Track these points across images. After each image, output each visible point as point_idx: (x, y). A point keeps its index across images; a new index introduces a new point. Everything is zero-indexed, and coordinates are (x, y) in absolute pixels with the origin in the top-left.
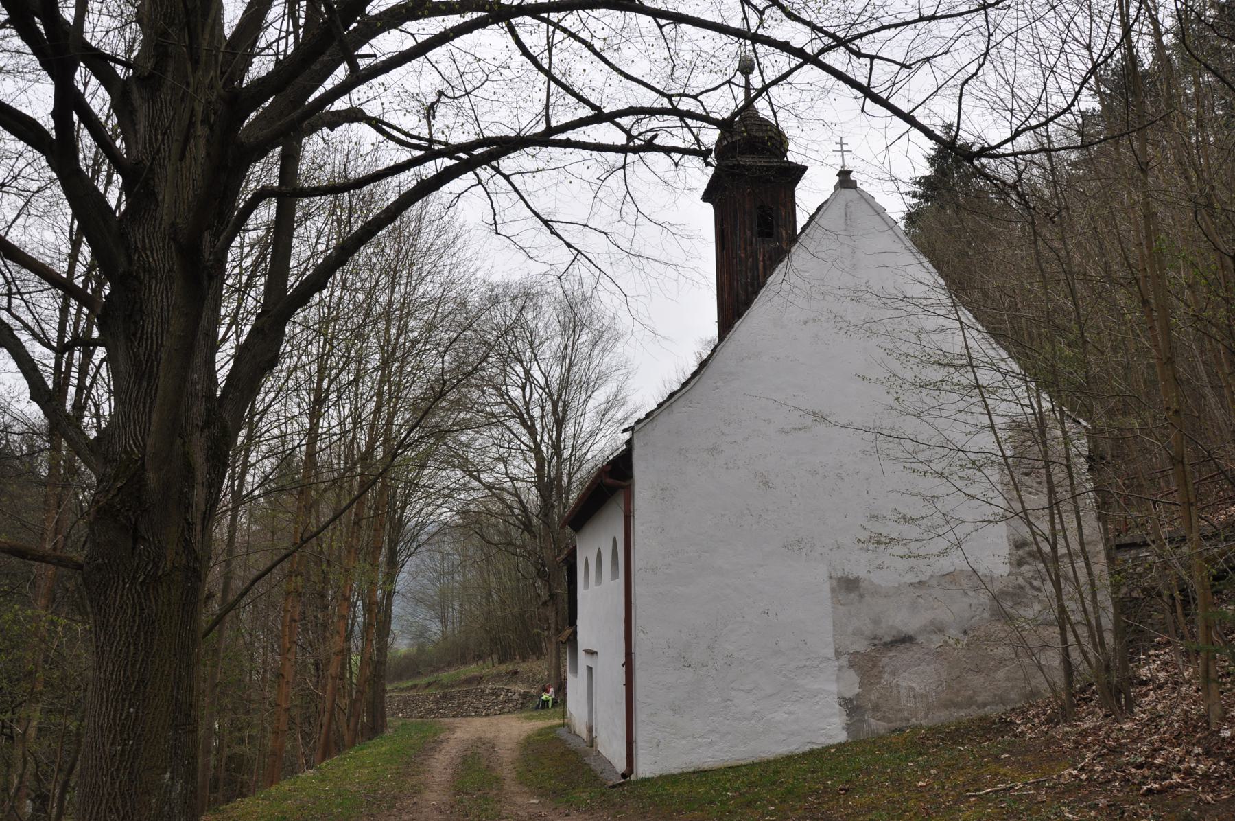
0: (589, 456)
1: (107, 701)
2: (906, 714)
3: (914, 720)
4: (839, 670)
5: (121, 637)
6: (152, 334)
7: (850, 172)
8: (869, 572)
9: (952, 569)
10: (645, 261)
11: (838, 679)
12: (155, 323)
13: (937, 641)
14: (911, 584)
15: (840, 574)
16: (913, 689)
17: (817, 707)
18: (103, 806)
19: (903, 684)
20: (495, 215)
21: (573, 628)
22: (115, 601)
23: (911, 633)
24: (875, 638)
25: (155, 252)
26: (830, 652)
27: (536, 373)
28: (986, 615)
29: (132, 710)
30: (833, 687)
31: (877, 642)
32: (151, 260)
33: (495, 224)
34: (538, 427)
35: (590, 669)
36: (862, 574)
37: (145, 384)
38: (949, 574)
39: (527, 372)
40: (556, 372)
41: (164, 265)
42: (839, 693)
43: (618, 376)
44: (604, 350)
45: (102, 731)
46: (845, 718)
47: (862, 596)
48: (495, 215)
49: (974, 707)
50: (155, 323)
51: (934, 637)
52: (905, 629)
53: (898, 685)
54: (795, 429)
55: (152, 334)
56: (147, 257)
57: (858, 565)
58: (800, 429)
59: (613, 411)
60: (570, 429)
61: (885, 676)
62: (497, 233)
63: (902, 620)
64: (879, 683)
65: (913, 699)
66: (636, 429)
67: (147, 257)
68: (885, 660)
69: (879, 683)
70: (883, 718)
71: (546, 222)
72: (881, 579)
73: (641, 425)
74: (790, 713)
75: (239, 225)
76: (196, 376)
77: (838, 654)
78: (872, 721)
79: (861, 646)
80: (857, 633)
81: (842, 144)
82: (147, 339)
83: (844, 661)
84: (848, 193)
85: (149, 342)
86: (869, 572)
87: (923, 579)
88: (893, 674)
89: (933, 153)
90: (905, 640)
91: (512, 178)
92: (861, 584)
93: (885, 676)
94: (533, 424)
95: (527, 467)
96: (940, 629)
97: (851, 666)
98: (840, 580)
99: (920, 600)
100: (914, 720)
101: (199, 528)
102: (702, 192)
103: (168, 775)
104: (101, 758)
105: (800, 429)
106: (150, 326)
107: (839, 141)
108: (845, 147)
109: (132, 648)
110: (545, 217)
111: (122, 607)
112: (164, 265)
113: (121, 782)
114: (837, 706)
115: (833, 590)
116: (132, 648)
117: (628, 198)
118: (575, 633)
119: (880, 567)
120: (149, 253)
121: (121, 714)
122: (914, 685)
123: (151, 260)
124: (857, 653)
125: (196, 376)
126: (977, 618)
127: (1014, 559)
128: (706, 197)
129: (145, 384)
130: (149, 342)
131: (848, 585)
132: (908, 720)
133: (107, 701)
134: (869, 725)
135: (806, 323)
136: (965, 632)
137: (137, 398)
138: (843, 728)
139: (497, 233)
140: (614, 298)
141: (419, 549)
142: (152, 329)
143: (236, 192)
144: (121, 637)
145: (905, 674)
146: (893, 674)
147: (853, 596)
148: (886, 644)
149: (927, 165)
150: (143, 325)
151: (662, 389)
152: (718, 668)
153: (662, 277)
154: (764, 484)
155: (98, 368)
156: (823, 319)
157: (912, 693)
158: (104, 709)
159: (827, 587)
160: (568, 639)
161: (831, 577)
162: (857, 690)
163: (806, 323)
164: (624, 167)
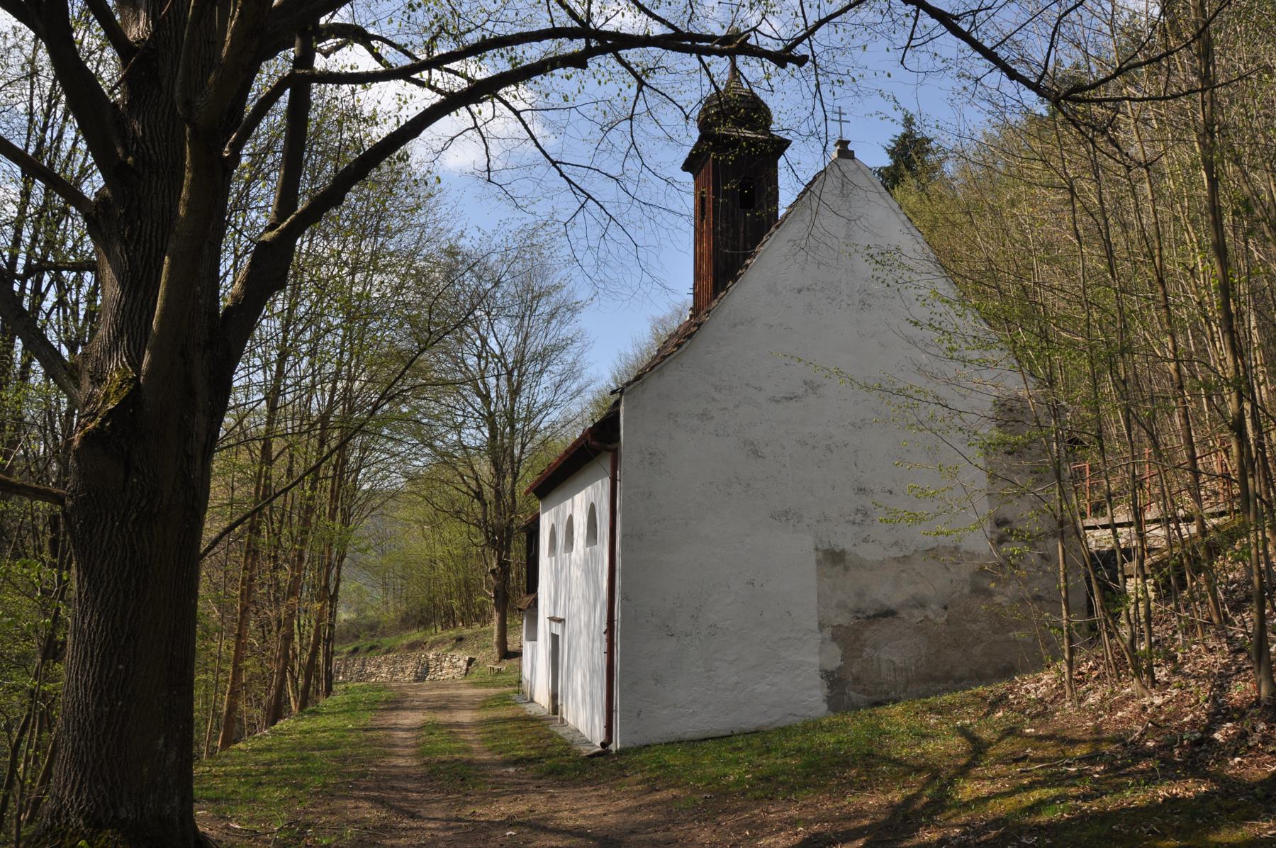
0: (542, 426)
1: (92, 656)
2: (885, 687)
3: (893, 693)
4: (822, 643)
5: (109, 583)
6: (151, 236)
7: (848, 142)
8: (855, 545)
9: (935, 545)
10: (655, 210)
11: (820, 653)
12: (155, 225)
13: (918, 615)
14: (895, 558)
15: (826, 546)
16: (893, 662)
17: (800, 679)
18: (88, 774)
19: (884, 656)
20: (489, 161)
21: (531, 597)
22: (102, 542)
23: (893, 607)
24: (858, 612)
25: (156, 143)
26: (814, 625)
27: (492, 343)
28: (966, 591)
29: (121, 667)
30: (816, 660)
31: (860, 615)
32: (152, 152)
33: (489, 170)
34: (493, 395)
35: (555, 638)
36: (848, 546)
37: (141, 294)
38: (933, 549)
39: (484, 341)
40: (513, 341)
41: (167, 159)
42: (821, 665)
43: (573, 349)
44: (562, 322)
45: (86, 691)
46: (826, 690)
47: (847, 569)
48: (489, 161)
49: (951, 682)
50: (155, 225)
51: (916, 612)
52: (887, 603)
53: (879, 659)
54: (786, 398)
55: (151, 236)
56: (148, 149)
57: (844, 539)
58: (791, 399)
59: (568, 383)
60: (523, 400)
61: (867, 649)
62: (489, 180)
63: (885, 593)
64: (861, 656)
65: (892, 673)
66: (626, 390)
67: (148, 149)
68: (867, 634)
69: (861, 656)
70: (864, 691)
71: (554, 163)
72: (869, 553)
73: (631, 386)
74: (773, 685)
75: (247, 132)
76: (199, 288)
77: (821, 626)
78: (852, 693)
79: (844, 619)
80: (841, 605)
81: (840, 114)
82: (145, 242)
83: (827, 633)
84: (846, 164)
85: (148, 245)
86: (855, 545)
87: (908, 554)
88: (875, 647)
89: (893, 145)
90: (889, 613)
91: (522, 115)
92: (847, 557)
93: (867, 649)
94: (488, 392)
95: (479, 436)
96: (922, 604)
97: (834, 638)
98: (826, 552)
99: (904, 575)
100: (893, 693)
101: (199, 462)
102: (682, 161)
103: (161, 741)
104: (85, 721)
105: (791, 399)
106: (149, 228)
107: (837, 110)
108: (843, 118)
109: (121, 596)
110: (554, 158)
111: (110, 549)
112: (167, 159)
113: (108, 749)
114: (819, 678)
115: (819, 562)
116: (121, 596)
117: (633, 151)
118: (536, 601)
119: (865, 540)
120: (149, 145)
121: (109, 672)
122: (894, 659)
123: (152, 152)
124: (840, 626)
125: (199, 288)
126: (958, 594)
127: (995, 536)
128: (687, 166)
129: (141, 294)
130: (148, 245)
131: (834, 558)
132: (888, 694)
133: (92, 656)
134: (850, 698)
135: (800, 291)
136: (946, 608)
137: (131, 310)
138: (824, 701)
139: (489, 180)
140: (622, 249)
141: (373, 513)
142: (151, 231)
143: (247, 87)
144: (109, 583)
145: (886, 648)
146: (875, 647)
147: (839, 568)
148: (868, 618)
149: (888, 156)
150: (141, 226)
151: (618, 363)
152: (702, 638)
153: (672, 227)
154: (753, 453)
155: (48, 315)
156: (817, 288)
157: (892, 667)
158: (88, 665)
159: (813, 557)
160: (529, 607)
161: (817, 549)
162: (839, 663)
163: (800, 291)
164: (631, 118)
